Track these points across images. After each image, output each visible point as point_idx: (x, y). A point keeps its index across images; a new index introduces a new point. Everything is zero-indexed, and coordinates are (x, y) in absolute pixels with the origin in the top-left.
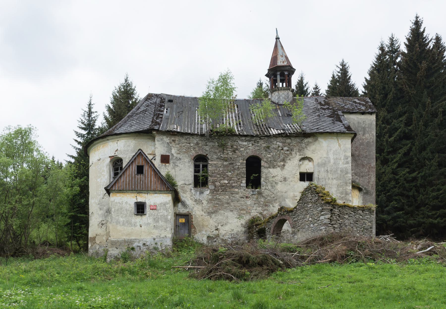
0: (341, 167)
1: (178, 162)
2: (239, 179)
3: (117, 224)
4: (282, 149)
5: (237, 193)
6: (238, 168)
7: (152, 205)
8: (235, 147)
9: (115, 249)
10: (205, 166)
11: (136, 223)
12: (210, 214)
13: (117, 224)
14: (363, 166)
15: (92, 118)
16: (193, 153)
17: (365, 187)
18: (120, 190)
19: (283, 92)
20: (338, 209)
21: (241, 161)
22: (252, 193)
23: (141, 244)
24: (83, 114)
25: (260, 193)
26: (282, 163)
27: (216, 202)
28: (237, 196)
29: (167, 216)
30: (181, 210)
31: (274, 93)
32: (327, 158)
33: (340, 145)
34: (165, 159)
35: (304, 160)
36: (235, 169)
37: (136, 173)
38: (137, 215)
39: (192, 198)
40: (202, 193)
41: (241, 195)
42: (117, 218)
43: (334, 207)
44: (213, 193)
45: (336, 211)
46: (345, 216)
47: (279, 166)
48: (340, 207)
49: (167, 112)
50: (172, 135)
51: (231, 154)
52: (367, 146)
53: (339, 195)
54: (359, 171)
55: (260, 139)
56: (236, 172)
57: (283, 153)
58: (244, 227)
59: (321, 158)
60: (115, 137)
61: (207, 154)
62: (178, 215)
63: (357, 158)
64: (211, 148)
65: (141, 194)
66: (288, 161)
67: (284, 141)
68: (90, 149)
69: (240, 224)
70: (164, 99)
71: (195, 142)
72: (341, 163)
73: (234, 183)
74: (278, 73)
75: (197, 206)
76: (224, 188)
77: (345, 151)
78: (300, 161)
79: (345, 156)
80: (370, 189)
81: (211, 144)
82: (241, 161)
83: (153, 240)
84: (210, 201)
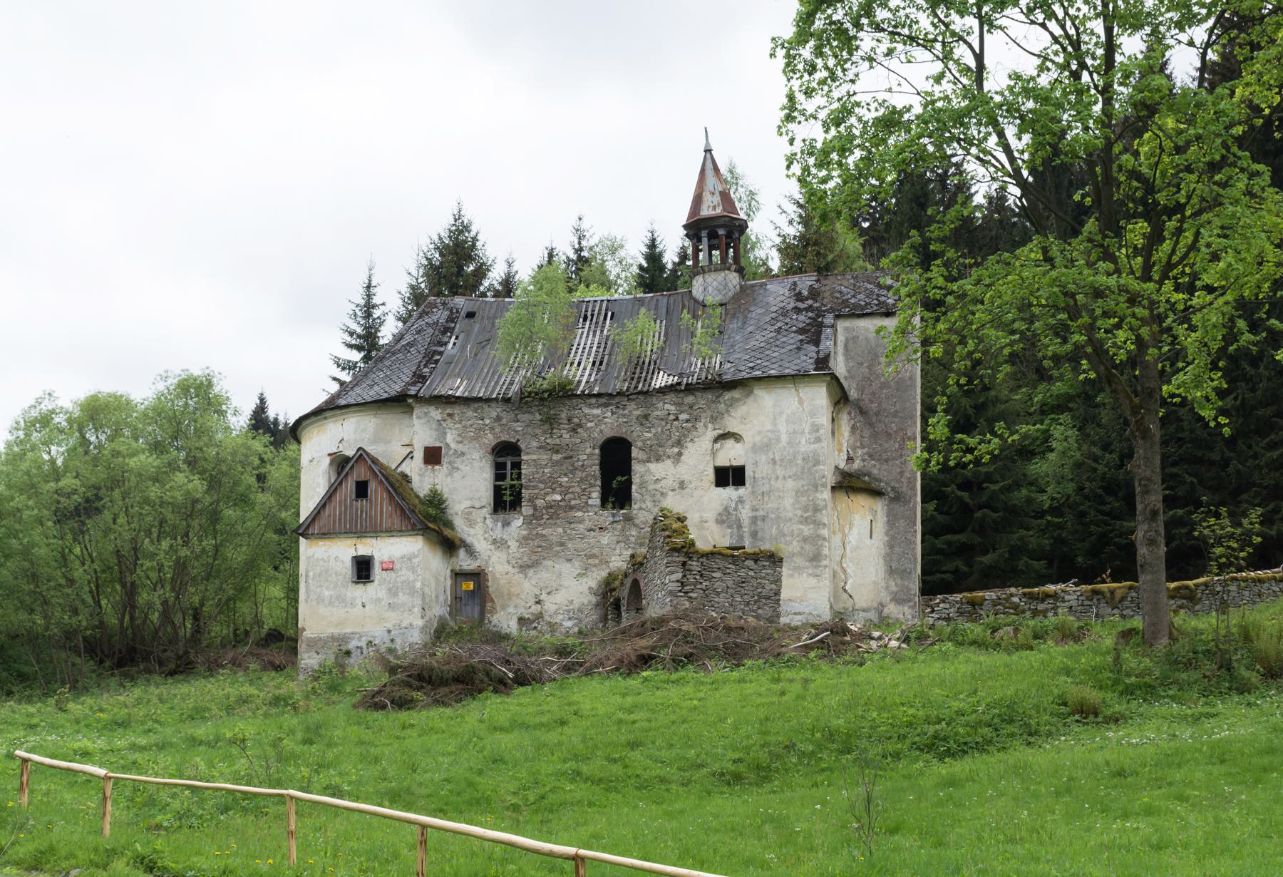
0: (803, 449)
1: (459, 460)
2: (584, 490)
3: (318, 603)
4: (677, 419)
5: (581, 521)
6: (583, 466)
7: (386, 560)
8: (576, 420)
9: (315, 655)
10: (517, 465)
11: (354, 599)
12: (523, 568)
13: (318, 603)
14: (889, 435)
15: (374, 320)
16: (490, 440)
17: (892, 484)
18: (324, 534)
19: (713, 275)
20: (698, 561)
21: (589, 451)
22: (611, 519)
23: (363, 644)
24: (351, 312)
25: (628, 519)
26: (676, 450)
27: (536, 542)
28: (581, 527)
29: (414, 581)
30: (464, 562)
31: (697, 277)
32: (773, 431)
33: (801, 402)
34: (433, 456)
35: (724, 439)
36: (576, 469)
37: (354, 496)
38: (357, 583)
39: (487, 535)
40: (506, 524)
41: (588, 524)
42: (318, 590)
43: (690, 558)
44: (530, 523)
45: (695, 565)
46: (714, 575)
47: (669, 457)
48: (702, 556)
49: (454, 344)
50: (447, 403)
51: (568, 436)
52: (898, 390)
53: (799, 513)
54: (879, 449)
55: (629, 399)
56: (579, 474)
57: (677, 428)
58: (595, 594)
59: (760, 432)
60: (338, 412)
61: (518, 440)
62: (458, 575)
63: (874, 419)
64: (527, 426)
65: (364, 540)
66: (689, 445)
67: (680, 401)
68: (309, 425)
69: (587, 586)
70: (457, 312)
71: (494, 414)
72: (803, 442)
73: (575, 499)
74: (704, 233)
75: (497, 553)
76: (554, 512)
77: (813, 414)
78: (716, 440)
79: (813, 425)
80: (904, 489)
81: (526, 417)
82: (589, 451)
83: (386, 633)
84: (524, 541)
